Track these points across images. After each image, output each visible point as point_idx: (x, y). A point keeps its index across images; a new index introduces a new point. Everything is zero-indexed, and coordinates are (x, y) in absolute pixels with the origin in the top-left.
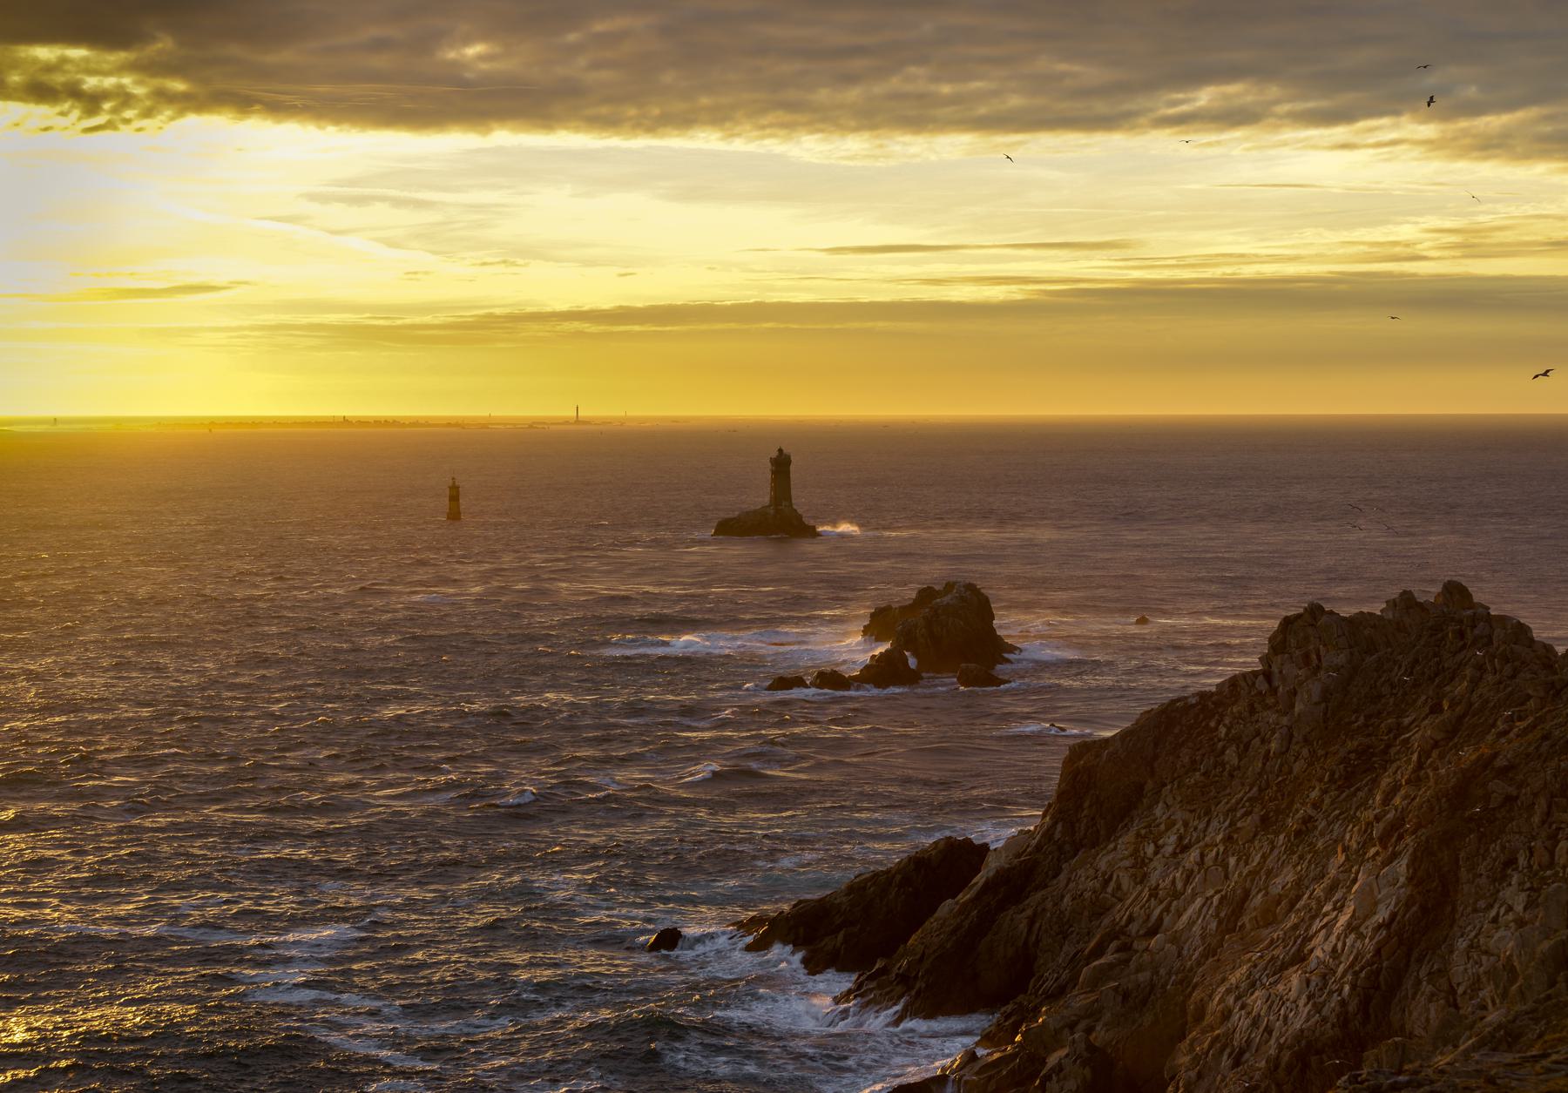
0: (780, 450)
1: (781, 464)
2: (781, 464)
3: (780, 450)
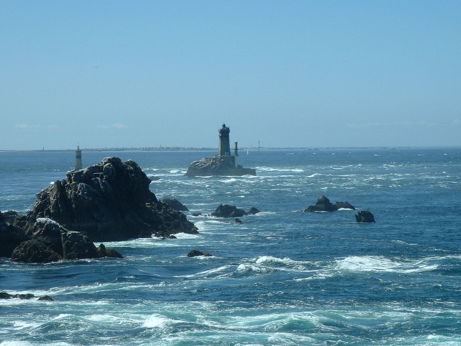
0: (224, 126)
1: (225, 133)
2: (225, 133)
3: (224, 126)
